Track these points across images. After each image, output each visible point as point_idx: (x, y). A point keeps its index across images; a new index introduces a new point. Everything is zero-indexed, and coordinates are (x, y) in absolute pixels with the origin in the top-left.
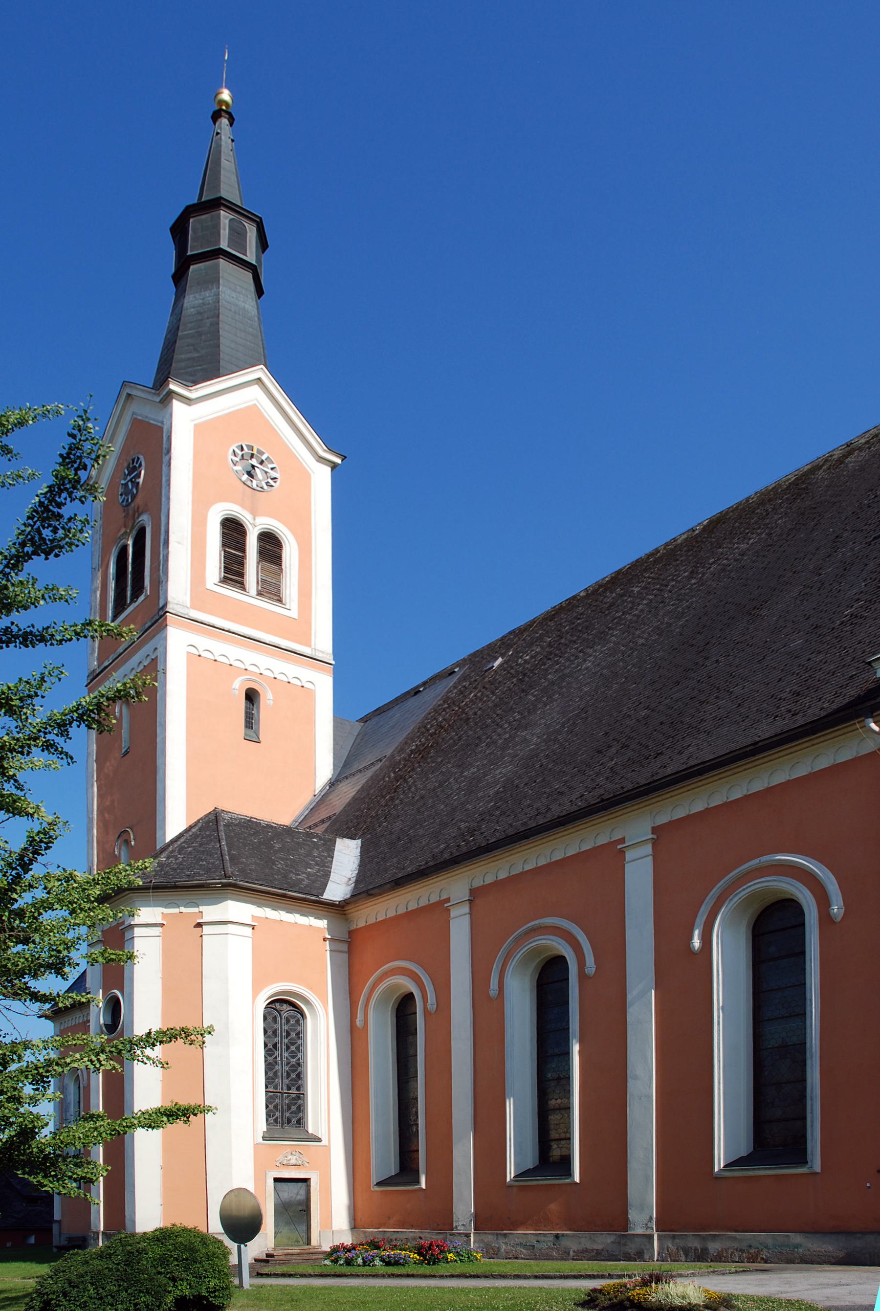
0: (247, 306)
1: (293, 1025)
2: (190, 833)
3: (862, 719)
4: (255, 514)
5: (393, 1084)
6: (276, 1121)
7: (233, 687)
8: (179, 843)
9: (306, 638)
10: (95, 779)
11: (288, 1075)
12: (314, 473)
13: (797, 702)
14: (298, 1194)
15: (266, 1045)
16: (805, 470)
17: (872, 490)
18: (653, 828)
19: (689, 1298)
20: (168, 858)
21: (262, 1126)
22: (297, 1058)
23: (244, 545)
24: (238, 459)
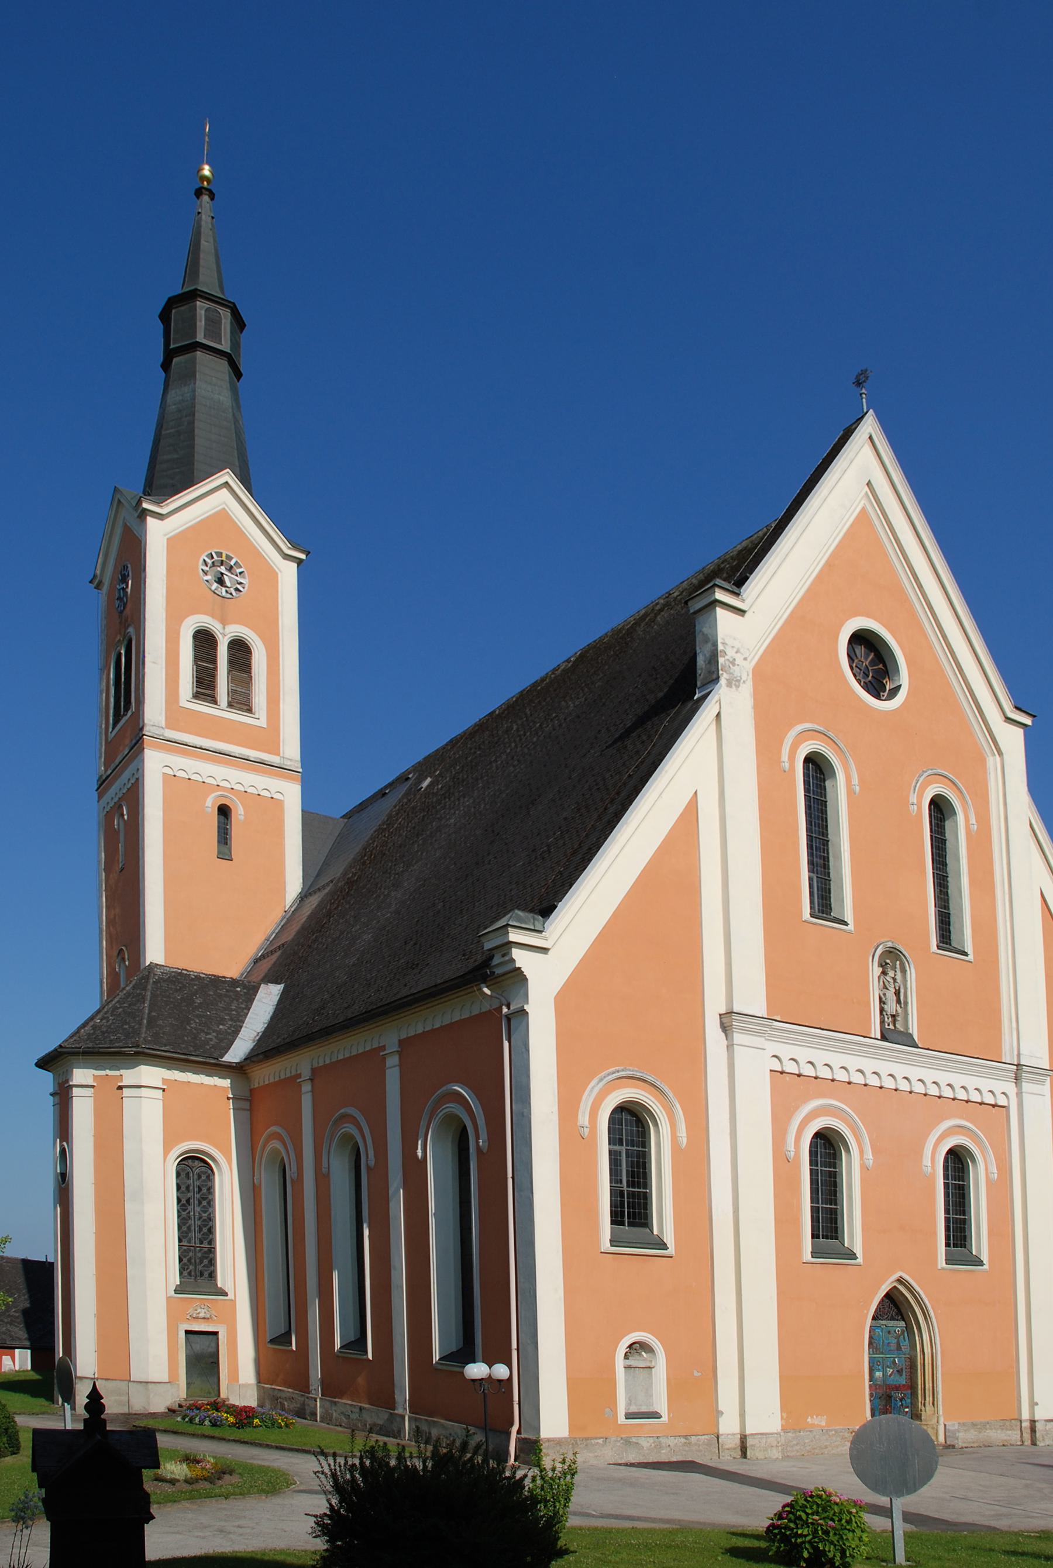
0: (221, 398)
1: (204, 1181)
2: (125, 992)
4: (224, 622)
5: (282, 1246)
6: (190, 1274)
7: (207, 805)
8: (114, 1002)
9: (274, 747)
10: (104, 888)
11: (200, 1230)
12: (280, 571)
14: (209, 1346)
15: (179, 1200)
18: (399, 1040)
20: (101, 1020)
21: (175, 1279)
22: (208, 1213)
23: (216, 656)
24: (207, 569)
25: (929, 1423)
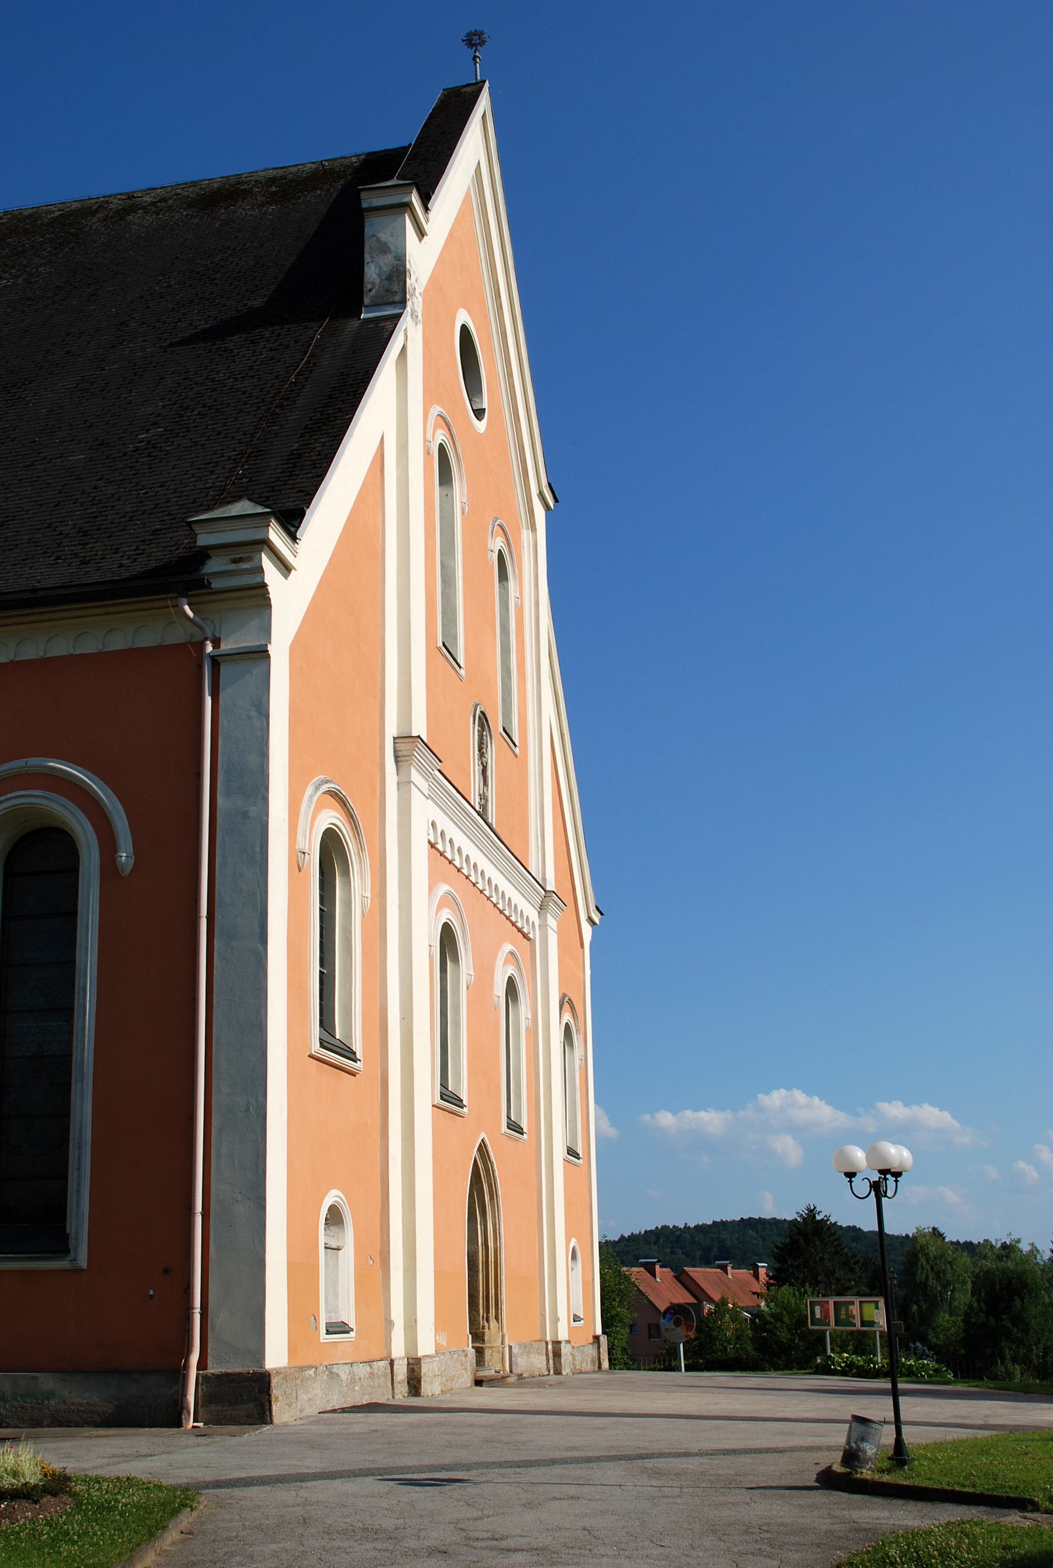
3: (176, 595)
13: (85, 544)
16: (73, 207)
17: (165, 275)
19: (23, 1475)
25: (493, 1344)
